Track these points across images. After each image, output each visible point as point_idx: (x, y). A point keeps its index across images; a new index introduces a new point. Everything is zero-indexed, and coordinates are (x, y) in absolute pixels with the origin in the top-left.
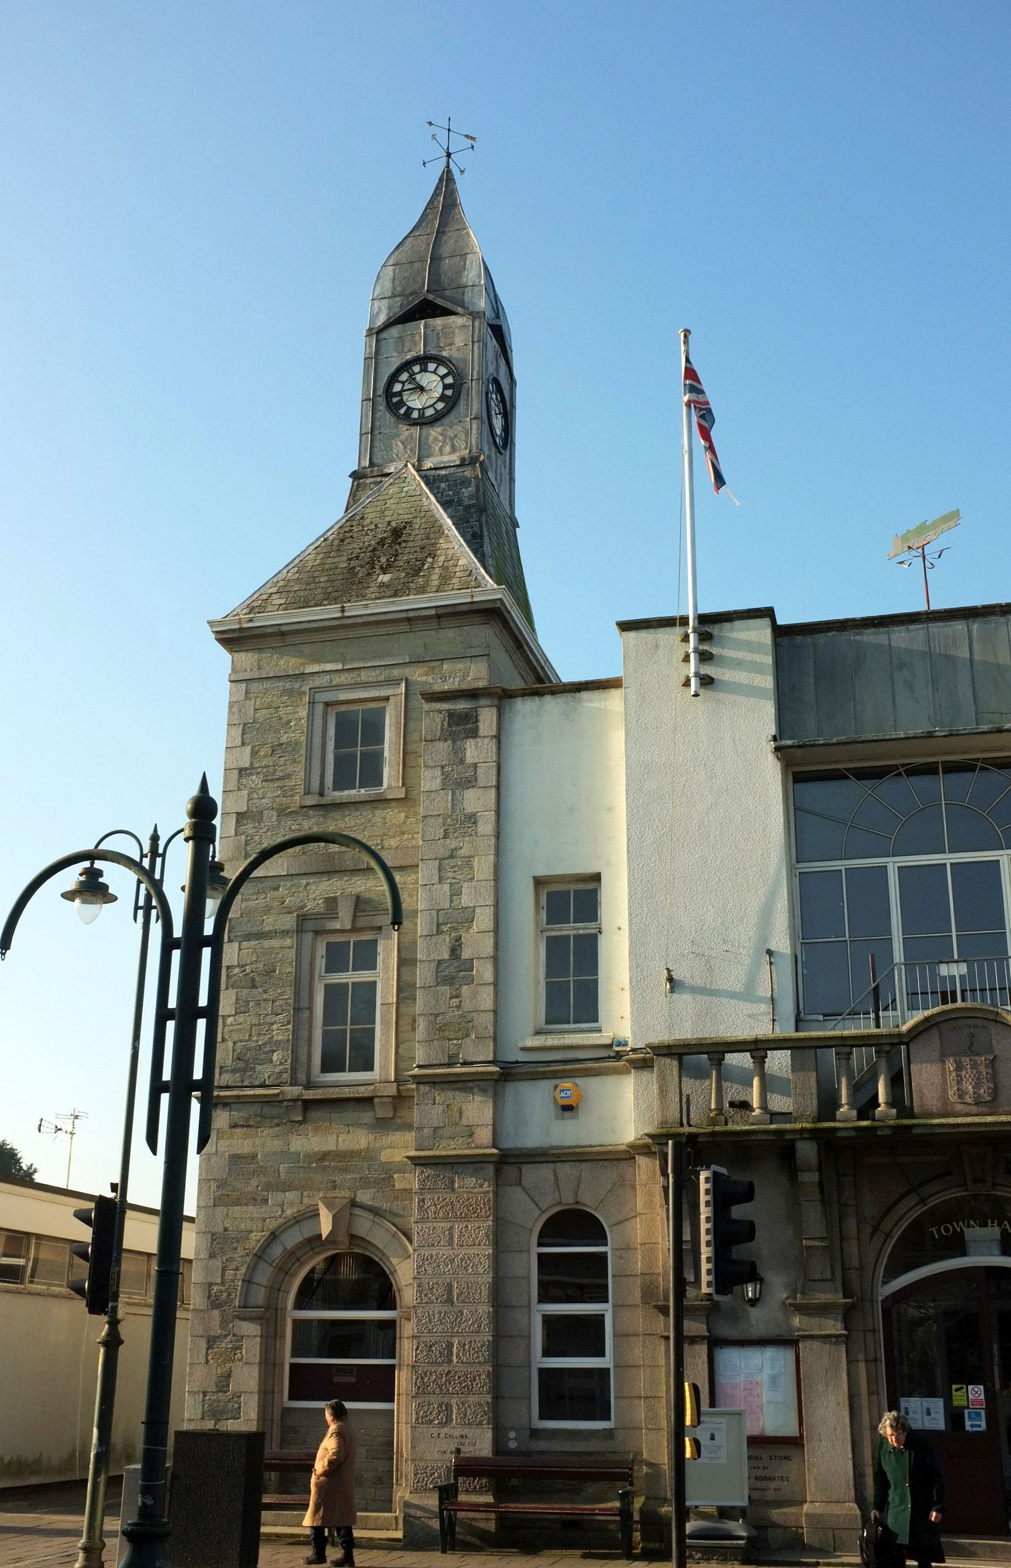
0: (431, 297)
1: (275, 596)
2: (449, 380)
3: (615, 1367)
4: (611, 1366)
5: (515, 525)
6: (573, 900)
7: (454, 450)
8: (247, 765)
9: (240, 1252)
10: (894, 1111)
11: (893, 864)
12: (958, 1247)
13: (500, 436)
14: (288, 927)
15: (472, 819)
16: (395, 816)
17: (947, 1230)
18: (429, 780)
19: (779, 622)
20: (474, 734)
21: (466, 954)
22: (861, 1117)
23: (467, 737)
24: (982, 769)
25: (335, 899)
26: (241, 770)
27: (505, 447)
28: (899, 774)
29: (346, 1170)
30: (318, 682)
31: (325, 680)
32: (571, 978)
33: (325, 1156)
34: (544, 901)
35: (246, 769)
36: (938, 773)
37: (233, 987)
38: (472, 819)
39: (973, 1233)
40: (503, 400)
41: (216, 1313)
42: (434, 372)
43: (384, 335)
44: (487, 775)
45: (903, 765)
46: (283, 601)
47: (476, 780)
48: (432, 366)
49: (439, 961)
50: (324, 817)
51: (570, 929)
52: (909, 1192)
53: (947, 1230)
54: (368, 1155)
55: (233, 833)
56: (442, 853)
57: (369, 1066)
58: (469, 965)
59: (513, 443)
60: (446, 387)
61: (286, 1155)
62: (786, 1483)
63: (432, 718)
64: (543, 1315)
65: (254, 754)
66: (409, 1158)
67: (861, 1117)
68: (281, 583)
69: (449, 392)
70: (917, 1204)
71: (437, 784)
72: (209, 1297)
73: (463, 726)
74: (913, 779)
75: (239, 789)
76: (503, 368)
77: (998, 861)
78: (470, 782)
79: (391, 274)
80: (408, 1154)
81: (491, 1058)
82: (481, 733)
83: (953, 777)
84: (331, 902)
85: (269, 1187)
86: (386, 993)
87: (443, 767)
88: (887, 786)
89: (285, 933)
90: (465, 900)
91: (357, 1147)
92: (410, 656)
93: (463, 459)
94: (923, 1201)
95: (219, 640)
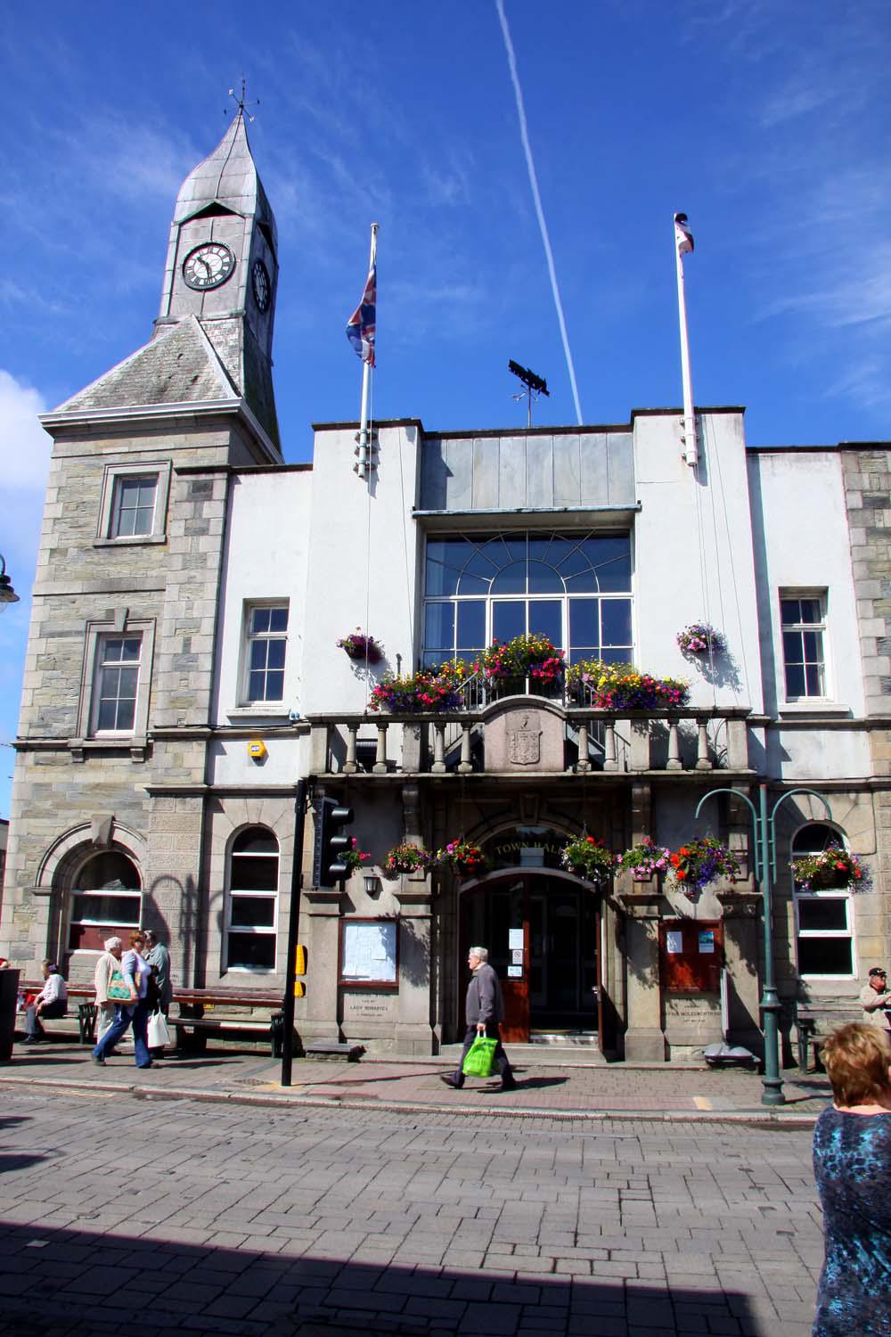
0: (218, 201)
1: (87, 400)
2: (227, 260)
3: (859, 937)
4: (277, 933)
5: (270, 363)
6: (268, 616)
7: (226, 308)
8: (59, 516)
9: (38, 849)
10: (471, 767)
11: (489, 600)
12: (516, 859)
13: (263, 302)
14: (80, 629)
15: (203, 558)
16: (156, 553)
17: (507, 848)
18: (176, 529)
19: (426, 430)
20: (209, 498)
21: (193, 650)
22: (448, 770)
23: (204, 500)
24: (556, 539)
25: (113, 611)
26: (55, 519)
27: (266, 309)
28: (499, 540)
29: (109, 796)
30: (111, 459)
31: (117, 459)
32: (266, 670)
33: (98, 786)
34: (252, 616)
35: (59, 519)
36: (525, 541)
37: (41, 669)
38: (203, 558)
39: (525, 851)
40: (267, 278)
41: (21, 889)
42: (217, 254)
43: (186, 226)
44: (217, 527)
45: (502, 532)
46: (91, 403)
47: (208, 529)
48: (216, 250)
49: (175, 654)
50: (110, 554)
51: (268, 635)
52: (481, 823)
53: (507, 848)
54: (126, 787)
55: (47, 563)
56: (182, 579)
57: (130, 727)
58: (195, 658)
59: (273, 309)
60: (224, 264)
61: (71, 786)
62: (385, 1011)
63: (182, 485)
64: (800, 901)
65: (66, 509)
66: (147, 789)
67: (448, 770)
68: (93, 391)
69: (226, 268)
70: (486, 831)
71: (182, 531)
72: (16, 879)
73: (201, 492)
74: (510, 544)
75: (53, 533)
76: (268, 255)
77: (560, 601)
78: (203, 531)
79: (193, 184)
80: (146, 786)
81: (206, 722)
82: (215, 497)
83: (538, 545)
84: (111, 613)
85: (58, 806)
86: (142, 678)
87: (186, 520)
88: (490, 548)
89: (78, 633)
90: (196, 614)
91: (118, 781)
92: (175, 444)
93: (231, 315)
94: (491, 829)
95: (45, 429)
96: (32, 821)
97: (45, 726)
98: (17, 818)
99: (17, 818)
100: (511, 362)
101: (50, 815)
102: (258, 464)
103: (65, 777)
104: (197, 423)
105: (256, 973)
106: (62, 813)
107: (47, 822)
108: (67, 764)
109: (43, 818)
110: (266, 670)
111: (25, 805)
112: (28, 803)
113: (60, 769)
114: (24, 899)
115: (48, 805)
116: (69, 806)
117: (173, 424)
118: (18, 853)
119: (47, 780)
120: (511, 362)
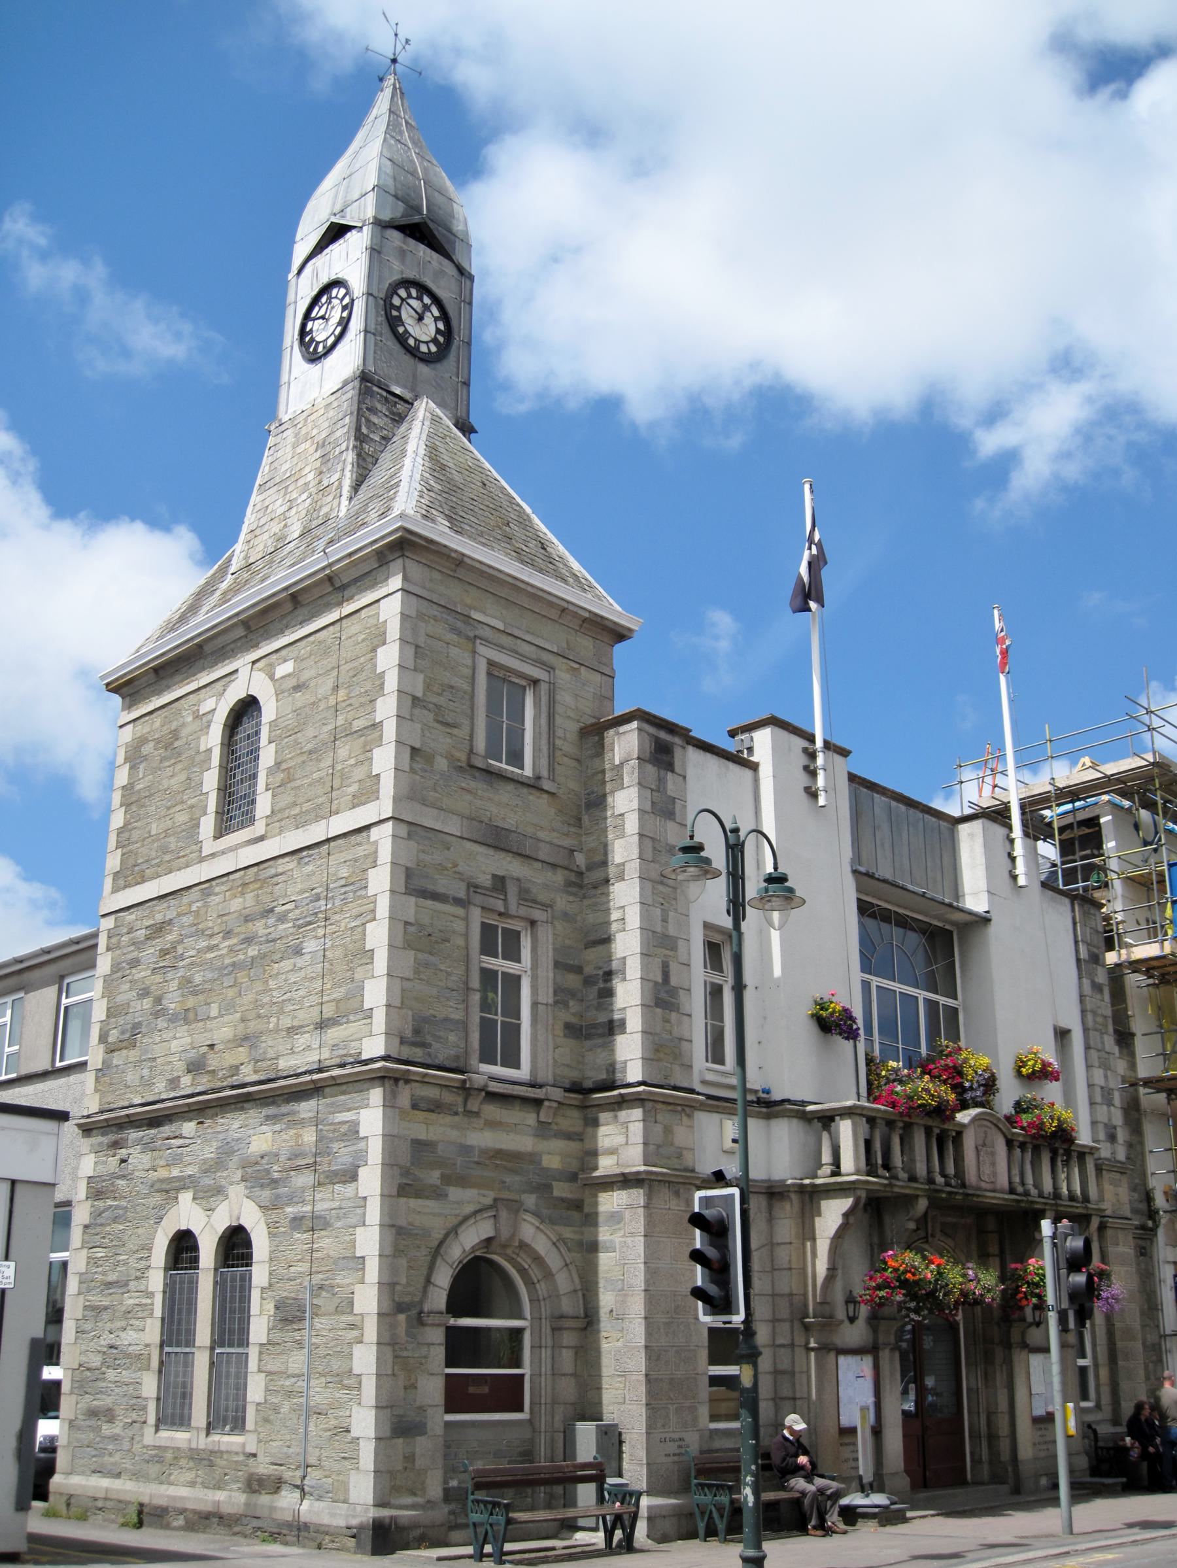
33: (499, 1154)
41: (402, 1317)
54: (532, 1158)
61: (466, 1150)
85: (447, 1180)
91: (523, 1149)
96: (413, 1202)
97: (423, 1045)
98: (390, 1196)
99: (390, 1196)
100: (850, 774)
101: (438, 1194)
102: (456, 525)
103: (454, 1135)
104: (581, 626)
105: (593, 1544)
106: (454, 1193)
107: (430, 1205)
108: (456, 1114)
109: (427, 1198)
110: (499, 1018)
111: (402, 1175)
112: (406, 1172)
113: (449, 1119)
114: (407, 1335)
115: (434, 1177)
116: (462, 1181)
117: (554, 614)
118: (394, 1256)
119: (432, 1136)
120: (850, 774)
